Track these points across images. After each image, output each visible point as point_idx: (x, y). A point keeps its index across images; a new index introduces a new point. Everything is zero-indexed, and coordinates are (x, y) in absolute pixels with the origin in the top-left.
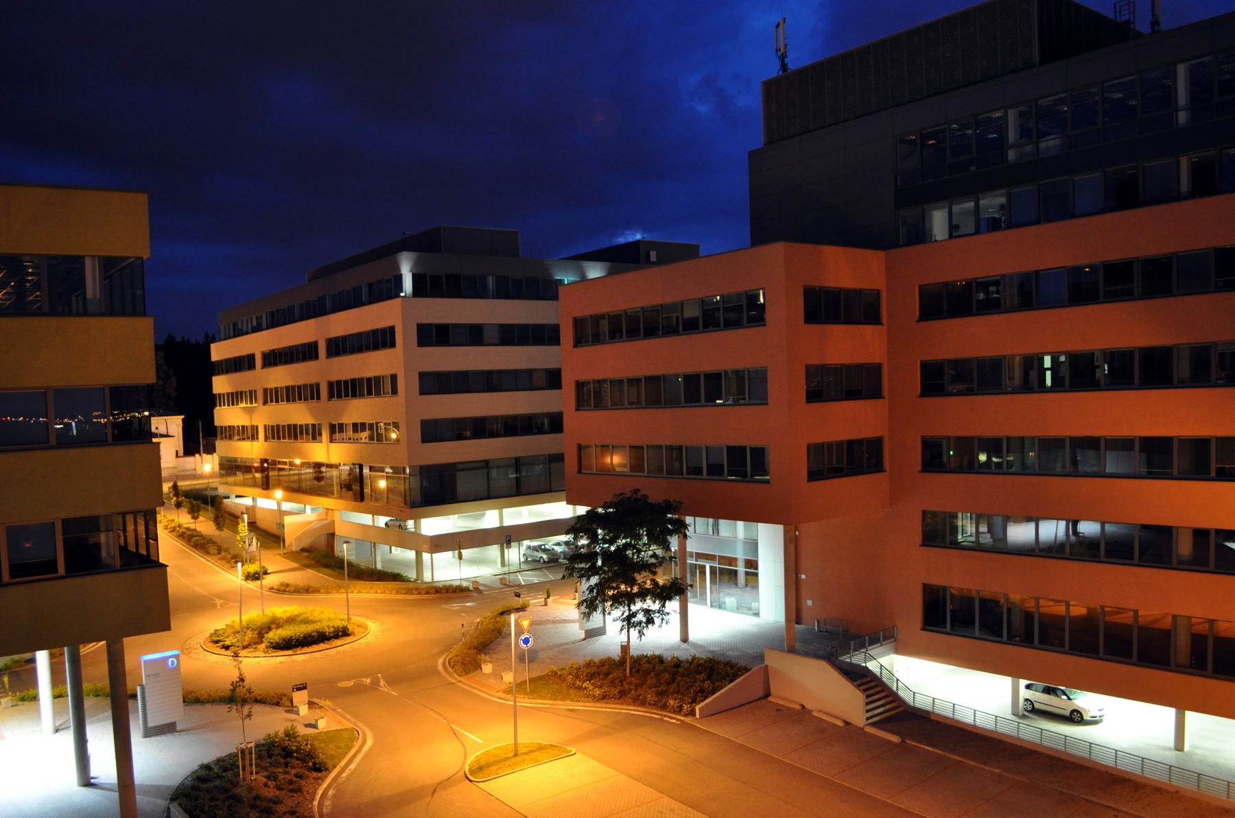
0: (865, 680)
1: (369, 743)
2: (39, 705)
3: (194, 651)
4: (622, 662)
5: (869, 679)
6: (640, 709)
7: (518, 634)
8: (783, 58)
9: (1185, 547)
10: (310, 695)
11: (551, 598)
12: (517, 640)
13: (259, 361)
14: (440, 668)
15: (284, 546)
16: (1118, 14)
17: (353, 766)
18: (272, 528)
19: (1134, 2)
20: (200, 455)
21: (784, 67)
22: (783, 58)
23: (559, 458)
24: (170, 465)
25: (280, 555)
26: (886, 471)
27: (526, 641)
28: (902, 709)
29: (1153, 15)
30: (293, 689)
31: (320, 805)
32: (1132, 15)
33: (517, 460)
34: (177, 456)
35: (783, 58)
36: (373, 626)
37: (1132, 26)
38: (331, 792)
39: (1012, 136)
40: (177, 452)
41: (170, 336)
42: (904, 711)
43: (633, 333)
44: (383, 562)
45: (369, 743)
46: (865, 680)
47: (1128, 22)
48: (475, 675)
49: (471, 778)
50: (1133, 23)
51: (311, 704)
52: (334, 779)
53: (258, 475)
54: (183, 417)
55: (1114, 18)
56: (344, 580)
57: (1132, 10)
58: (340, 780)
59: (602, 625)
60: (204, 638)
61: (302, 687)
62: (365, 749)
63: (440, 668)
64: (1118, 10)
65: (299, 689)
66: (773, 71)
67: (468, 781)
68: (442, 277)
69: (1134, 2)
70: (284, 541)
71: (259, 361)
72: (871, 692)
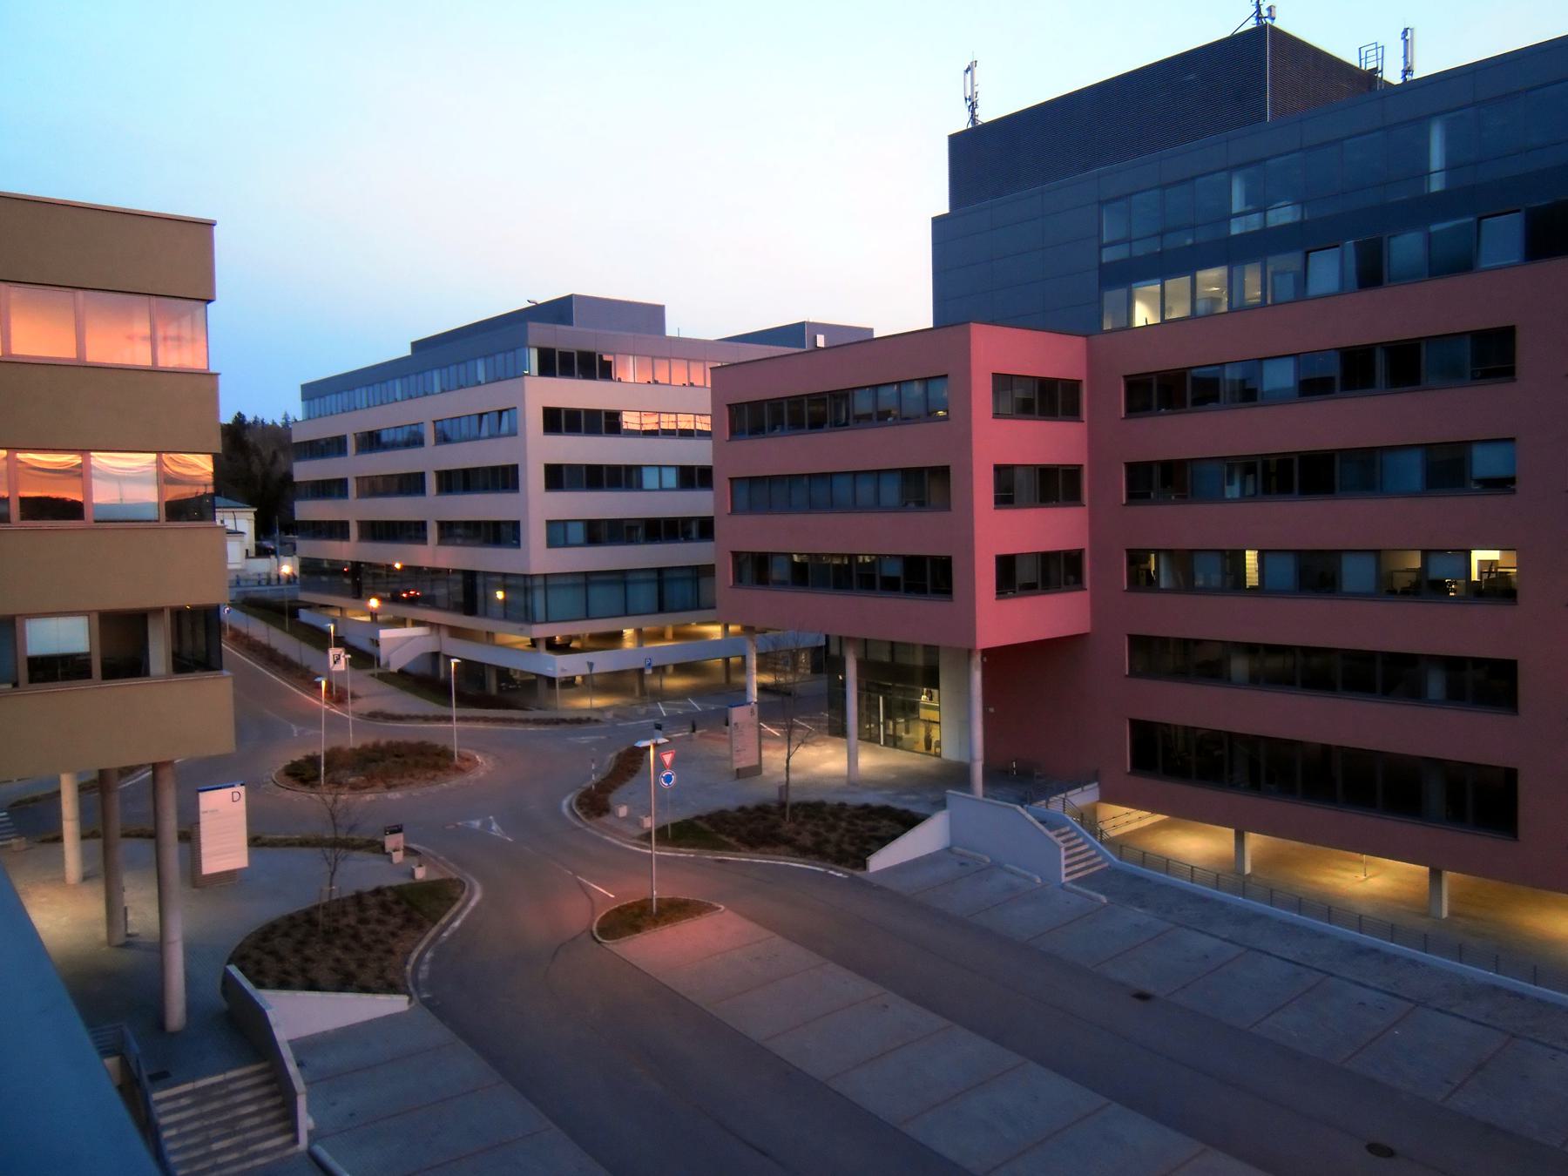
0: (1063, 830)
1: (477, 897)
2: (63, 847)
3: (263, 786)
4: (783, 805)
5: (1068, 829)
6: (801, 860)
7: (658, 773)
8: (973, 107)
9: (1436, 684)
10: (406, 840)
11: (698, 732)
12: (657, 782)
13: (351, 445)
14: (565, 810)
15: (379, 665)
16: (1363, 61)
17: (457, 924)
18: (364, 645)
19: (1383, 47)
20: (277, 557)
21: (973, 118)
22: (974, 109)
23: (707, 571)
24: (238, 567)
25: (373, 675)
26: (1084, 506)
27: (668, 779)
28: (1106, 864)
29: (1406, 63)
30: (386, 831)
31: (416, 969)
32: (1380, 61)
33: (660, 571)
34: (247, 556)
35: (973, 107)
36: (484, 764)
37: (1380, 75)
38: (428, 955)
39: (1237, 205)
40: (247, 551)
41: (239, 414)
42: (1110, 867)
43: (797, 425)
44: (284, 622)
45: (477, 897)
46: (1063, 830)
47: (1375, 70)
48: (607, 819)
49: (600, 939)
50: (1381, 71)
51: (409, 851)
52: (434, 940)
53: (348, 581)
54: (255, 510)
55: (1358, 66)
56: (451, 706)
57: (1380, 57)
58: (441, 941)
59: (756, 763)
60: (276, 771)
61: (397, 830)
62: (472, 904)
63: (565, 810)
64: (1363, 56)
65: (393, 832)
66: (962, 124)
67: (595, 943)
68: (573, 353)
69: (1383, 47)
70: (378, 660)
71: (351, 445)
72: (1072, 844)
